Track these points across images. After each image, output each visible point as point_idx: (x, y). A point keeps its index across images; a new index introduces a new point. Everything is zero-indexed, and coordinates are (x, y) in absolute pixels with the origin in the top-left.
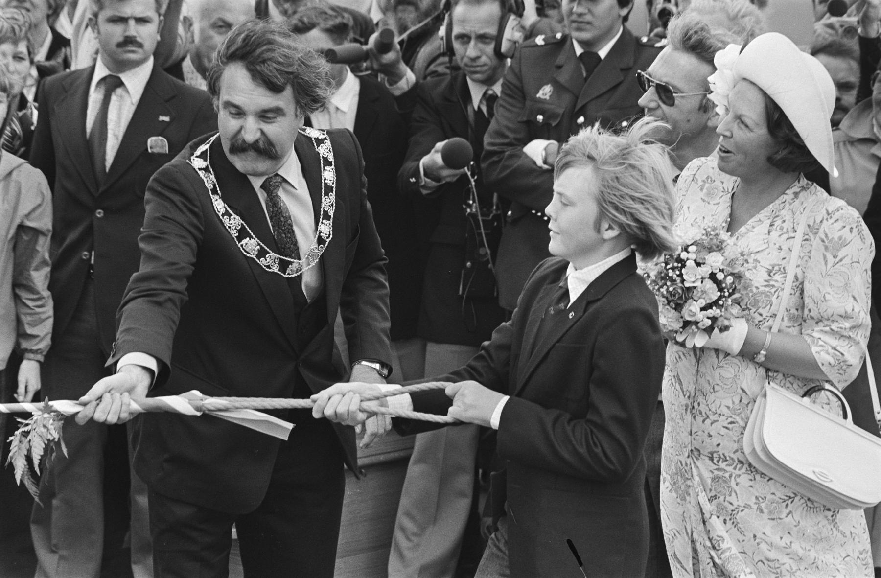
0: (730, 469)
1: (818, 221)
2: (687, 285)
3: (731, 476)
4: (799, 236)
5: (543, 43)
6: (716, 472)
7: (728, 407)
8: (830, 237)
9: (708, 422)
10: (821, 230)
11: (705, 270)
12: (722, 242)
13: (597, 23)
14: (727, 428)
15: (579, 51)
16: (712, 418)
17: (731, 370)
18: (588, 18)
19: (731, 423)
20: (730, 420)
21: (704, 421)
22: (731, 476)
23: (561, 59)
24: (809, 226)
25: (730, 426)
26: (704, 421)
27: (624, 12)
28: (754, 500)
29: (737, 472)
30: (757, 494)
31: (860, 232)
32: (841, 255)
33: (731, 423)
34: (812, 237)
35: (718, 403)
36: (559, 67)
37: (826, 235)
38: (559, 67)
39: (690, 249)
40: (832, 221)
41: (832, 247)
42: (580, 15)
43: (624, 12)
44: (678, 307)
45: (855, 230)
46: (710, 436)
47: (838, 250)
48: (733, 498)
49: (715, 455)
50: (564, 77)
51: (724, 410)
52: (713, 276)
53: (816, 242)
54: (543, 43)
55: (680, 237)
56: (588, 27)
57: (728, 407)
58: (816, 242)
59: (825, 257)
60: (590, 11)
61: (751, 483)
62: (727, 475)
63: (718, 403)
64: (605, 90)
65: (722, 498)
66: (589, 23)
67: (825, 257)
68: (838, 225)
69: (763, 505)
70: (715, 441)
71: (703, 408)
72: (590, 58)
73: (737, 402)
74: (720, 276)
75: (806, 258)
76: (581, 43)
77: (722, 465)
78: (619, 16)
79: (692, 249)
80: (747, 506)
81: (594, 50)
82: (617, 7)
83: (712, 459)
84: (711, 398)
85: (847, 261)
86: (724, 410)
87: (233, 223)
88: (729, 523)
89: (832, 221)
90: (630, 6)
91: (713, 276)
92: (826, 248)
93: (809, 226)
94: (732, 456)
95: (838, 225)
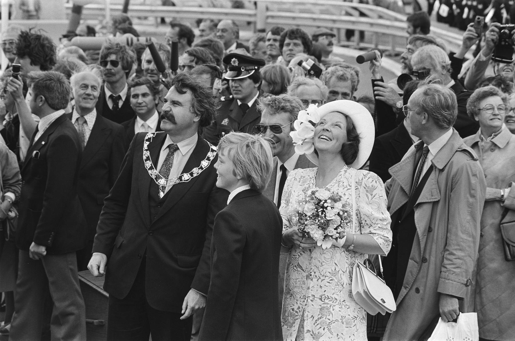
0: (331, 302)
1: (361, 179)
2: (328, 219)
3: (330, 306)
4: (353, 188)
5: (224, 100)
6: (322, 305)
7: (330, 273)
8: (368, 186)
9: (320, 280)
10: (363, 183)
11: (336, 211)
12: (341, 197)
13: (243, 91)
14: (329, 283)
15: (239, 103)
16: (322, 278)
17: (329, 254)
18: (240, 88)
19: (331, 280)
20: (331, 279)
21: (318, 280)
22: (330, 306)
23: (232, 107)
24: (356, 182)
25: (331, 282)
26: (318, 280)
27: (257, 85)
28: (340, 318)
29: (334, 304)
30: (342, 315)
31: (379, 182)
32: (374, 193)
33: (331, 280)
34: (359, 187)
35: (324, 271)
36: (231, 111)
37: (366, 185)
38: (231, 111)
39: (328, 201)
40: (367, 178)
41: (369, 190)
42: (236, 87)
43: (257, 85)
44: (324, 229)
45: (377, 182)
46: (321, 287)
47: (372, 191)
48: (330, 317)
49: (323, 297)
50: (233, 115)
51: (328, 274)
52: (339, 214)
53: (362, 189)
54: (224, 100)
55: (322, 196)
56: (240, 92)
57: (330, 273)
58: (362, 189)
59: (367, 195)
60: (240, 86)
61: (340, 309)
62: (329, 306)
63: (324, 271)
64: (251, 121)
65: (324, 317)
66: (240, 91)
67: (367, 195)
68: (370, 180)
69: (344, 320)
70: (323, 289)
71: (317, 274)
72: (244, 106)
73: (334, 270)
74: (341, 213)
75: (358, 197)
76: (241, 100)
77: (326, 301)
78: (255, 87)
79: (329, 201)
80: (337, 320)
81: (246, 103)
82: (253, 84)
83: (321, 299)
84: (321, 268)
85: (377, 196)
86: (328, 274)
87: (146, 154)
88: (326, 329)
89: (367, 178)
90: (260, 83)
91: (339, 214)
92: (367, 191)
93: (356, 182)
94: (332, 296)
95: (370, 180)
